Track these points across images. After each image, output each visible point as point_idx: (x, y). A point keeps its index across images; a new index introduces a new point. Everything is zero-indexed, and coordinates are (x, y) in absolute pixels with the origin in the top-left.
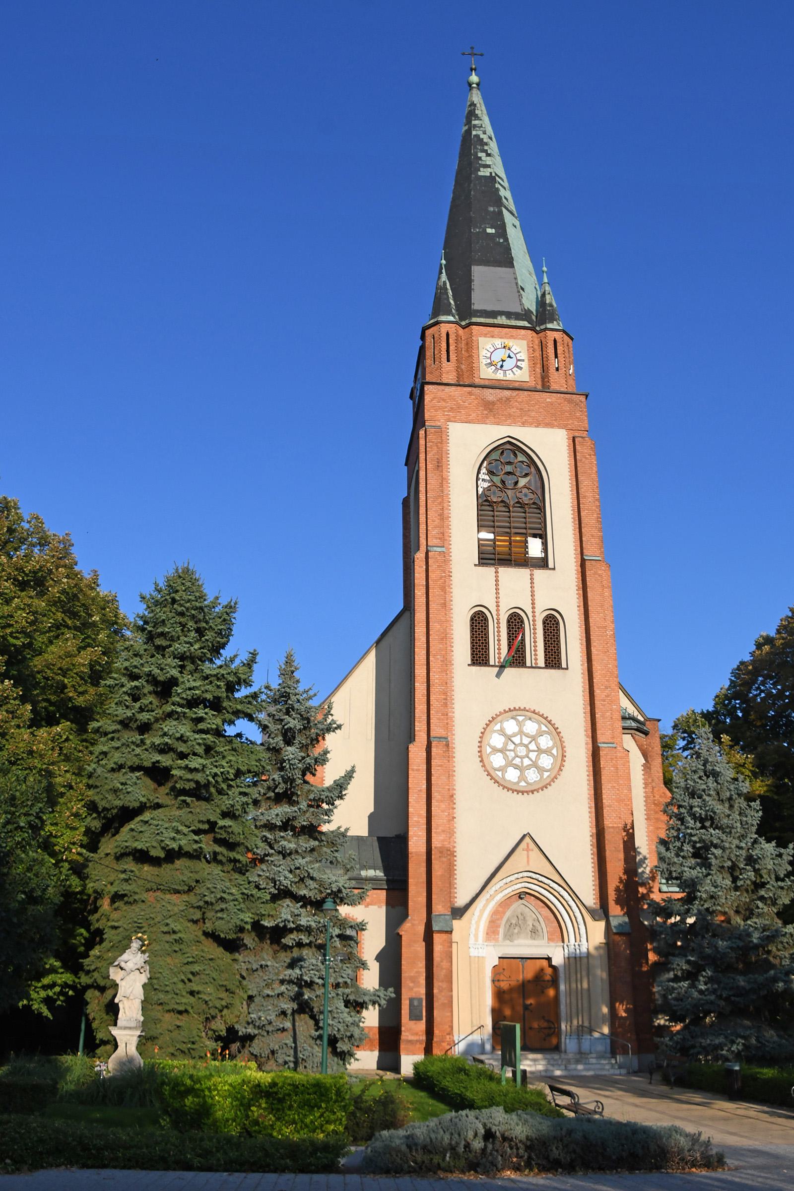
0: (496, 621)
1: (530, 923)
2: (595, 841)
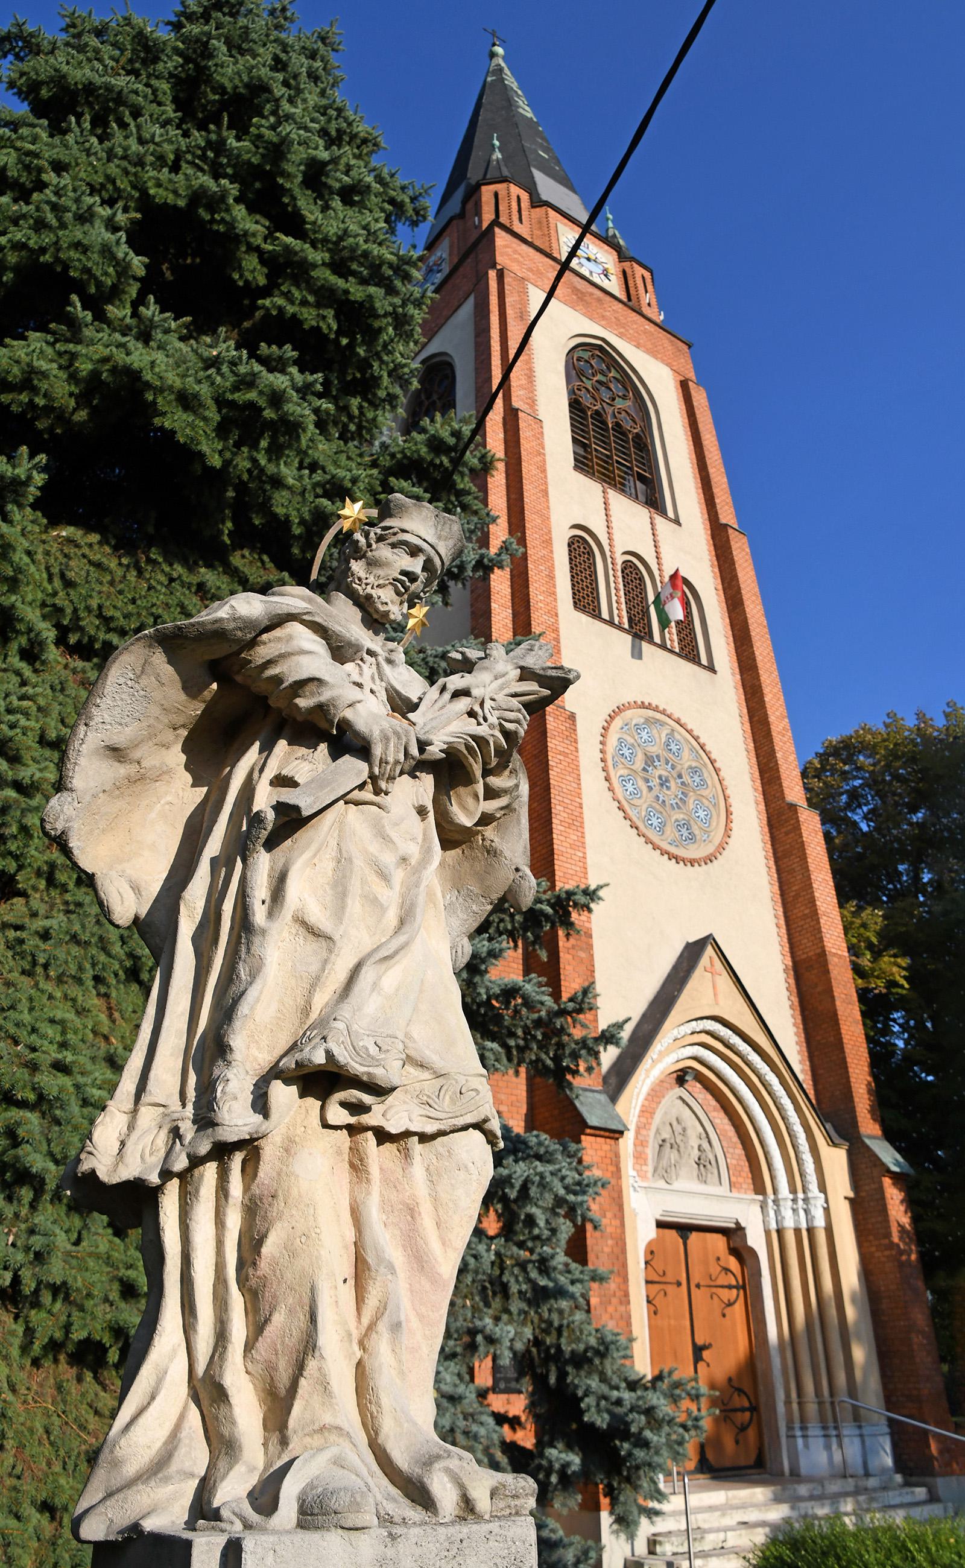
0: (609, 560)
1: (694, 1142)
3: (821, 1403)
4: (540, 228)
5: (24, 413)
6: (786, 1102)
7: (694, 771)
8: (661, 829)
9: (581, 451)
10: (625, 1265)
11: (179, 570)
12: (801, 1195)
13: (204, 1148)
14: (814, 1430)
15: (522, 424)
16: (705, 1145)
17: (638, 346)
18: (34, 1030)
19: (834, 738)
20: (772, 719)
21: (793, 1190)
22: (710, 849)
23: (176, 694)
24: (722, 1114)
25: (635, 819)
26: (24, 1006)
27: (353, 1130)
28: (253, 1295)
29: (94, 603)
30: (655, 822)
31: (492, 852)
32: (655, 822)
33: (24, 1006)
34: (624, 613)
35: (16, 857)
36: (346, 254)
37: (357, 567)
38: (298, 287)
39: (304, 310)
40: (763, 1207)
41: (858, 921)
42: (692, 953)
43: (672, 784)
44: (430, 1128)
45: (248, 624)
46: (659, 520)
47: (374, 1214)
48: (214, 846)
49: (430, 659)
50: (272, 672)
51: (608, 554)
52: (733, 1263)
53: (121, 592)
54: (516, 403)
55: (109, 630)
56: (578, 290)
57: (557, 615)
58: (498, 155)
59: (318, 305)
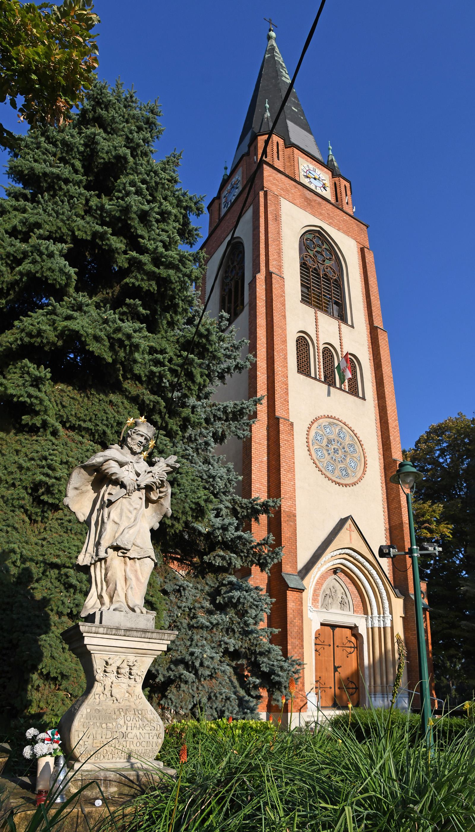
0: (316, 348)
1: (340, 595)
2: (388, 534)
3: (382, 687)
4: (289, 162)
5: (40, 345)
6: (379, 581)
7: (351, 445)
8: (333, 471)
9: (305, 290)
10: (302, 636)
11: (102, 396)
12: (382, 615)
13: (97, 559)
14: (379, 695)
15: (274, 281)
16: (344, 596)
17: (339, 230)
18: (69, 548)
19: (435, 424)
20: (390, 421)
21: (379, 613)
22: (355, 479)
23: (87, 476)
24: (352, 585)
25: (321, 467)
26: (66, 541)
27: (124, 557)
28: (107, 582)
29: (73, 413)
30: (330, 468)
31: (162, 505)
32: (330, 468)
33: (66, 541)
34: (322, 374)
35: (58, 499)
36: (158, 255)
37: (129, 439)
38: (139, 273)
39: (143, 283)
40: (367, 620)
41: (431, 509)
42: (342, 522)
43: (340, 452)
44: (139, 557)
45: (100, 463)
46: (343, 326)
47: (128, 570)
48: (98, 506)
49: (213, 411)
50: (106, 471)
51: (316, 345)
52: (353, 639)
53: (82, 407)
54: (272, 269)
55: (80, 421)
56: (308, 199)
57: (287, 377)
58: (268, 114)
59: (149, 280)
